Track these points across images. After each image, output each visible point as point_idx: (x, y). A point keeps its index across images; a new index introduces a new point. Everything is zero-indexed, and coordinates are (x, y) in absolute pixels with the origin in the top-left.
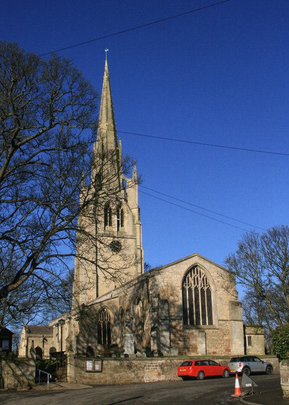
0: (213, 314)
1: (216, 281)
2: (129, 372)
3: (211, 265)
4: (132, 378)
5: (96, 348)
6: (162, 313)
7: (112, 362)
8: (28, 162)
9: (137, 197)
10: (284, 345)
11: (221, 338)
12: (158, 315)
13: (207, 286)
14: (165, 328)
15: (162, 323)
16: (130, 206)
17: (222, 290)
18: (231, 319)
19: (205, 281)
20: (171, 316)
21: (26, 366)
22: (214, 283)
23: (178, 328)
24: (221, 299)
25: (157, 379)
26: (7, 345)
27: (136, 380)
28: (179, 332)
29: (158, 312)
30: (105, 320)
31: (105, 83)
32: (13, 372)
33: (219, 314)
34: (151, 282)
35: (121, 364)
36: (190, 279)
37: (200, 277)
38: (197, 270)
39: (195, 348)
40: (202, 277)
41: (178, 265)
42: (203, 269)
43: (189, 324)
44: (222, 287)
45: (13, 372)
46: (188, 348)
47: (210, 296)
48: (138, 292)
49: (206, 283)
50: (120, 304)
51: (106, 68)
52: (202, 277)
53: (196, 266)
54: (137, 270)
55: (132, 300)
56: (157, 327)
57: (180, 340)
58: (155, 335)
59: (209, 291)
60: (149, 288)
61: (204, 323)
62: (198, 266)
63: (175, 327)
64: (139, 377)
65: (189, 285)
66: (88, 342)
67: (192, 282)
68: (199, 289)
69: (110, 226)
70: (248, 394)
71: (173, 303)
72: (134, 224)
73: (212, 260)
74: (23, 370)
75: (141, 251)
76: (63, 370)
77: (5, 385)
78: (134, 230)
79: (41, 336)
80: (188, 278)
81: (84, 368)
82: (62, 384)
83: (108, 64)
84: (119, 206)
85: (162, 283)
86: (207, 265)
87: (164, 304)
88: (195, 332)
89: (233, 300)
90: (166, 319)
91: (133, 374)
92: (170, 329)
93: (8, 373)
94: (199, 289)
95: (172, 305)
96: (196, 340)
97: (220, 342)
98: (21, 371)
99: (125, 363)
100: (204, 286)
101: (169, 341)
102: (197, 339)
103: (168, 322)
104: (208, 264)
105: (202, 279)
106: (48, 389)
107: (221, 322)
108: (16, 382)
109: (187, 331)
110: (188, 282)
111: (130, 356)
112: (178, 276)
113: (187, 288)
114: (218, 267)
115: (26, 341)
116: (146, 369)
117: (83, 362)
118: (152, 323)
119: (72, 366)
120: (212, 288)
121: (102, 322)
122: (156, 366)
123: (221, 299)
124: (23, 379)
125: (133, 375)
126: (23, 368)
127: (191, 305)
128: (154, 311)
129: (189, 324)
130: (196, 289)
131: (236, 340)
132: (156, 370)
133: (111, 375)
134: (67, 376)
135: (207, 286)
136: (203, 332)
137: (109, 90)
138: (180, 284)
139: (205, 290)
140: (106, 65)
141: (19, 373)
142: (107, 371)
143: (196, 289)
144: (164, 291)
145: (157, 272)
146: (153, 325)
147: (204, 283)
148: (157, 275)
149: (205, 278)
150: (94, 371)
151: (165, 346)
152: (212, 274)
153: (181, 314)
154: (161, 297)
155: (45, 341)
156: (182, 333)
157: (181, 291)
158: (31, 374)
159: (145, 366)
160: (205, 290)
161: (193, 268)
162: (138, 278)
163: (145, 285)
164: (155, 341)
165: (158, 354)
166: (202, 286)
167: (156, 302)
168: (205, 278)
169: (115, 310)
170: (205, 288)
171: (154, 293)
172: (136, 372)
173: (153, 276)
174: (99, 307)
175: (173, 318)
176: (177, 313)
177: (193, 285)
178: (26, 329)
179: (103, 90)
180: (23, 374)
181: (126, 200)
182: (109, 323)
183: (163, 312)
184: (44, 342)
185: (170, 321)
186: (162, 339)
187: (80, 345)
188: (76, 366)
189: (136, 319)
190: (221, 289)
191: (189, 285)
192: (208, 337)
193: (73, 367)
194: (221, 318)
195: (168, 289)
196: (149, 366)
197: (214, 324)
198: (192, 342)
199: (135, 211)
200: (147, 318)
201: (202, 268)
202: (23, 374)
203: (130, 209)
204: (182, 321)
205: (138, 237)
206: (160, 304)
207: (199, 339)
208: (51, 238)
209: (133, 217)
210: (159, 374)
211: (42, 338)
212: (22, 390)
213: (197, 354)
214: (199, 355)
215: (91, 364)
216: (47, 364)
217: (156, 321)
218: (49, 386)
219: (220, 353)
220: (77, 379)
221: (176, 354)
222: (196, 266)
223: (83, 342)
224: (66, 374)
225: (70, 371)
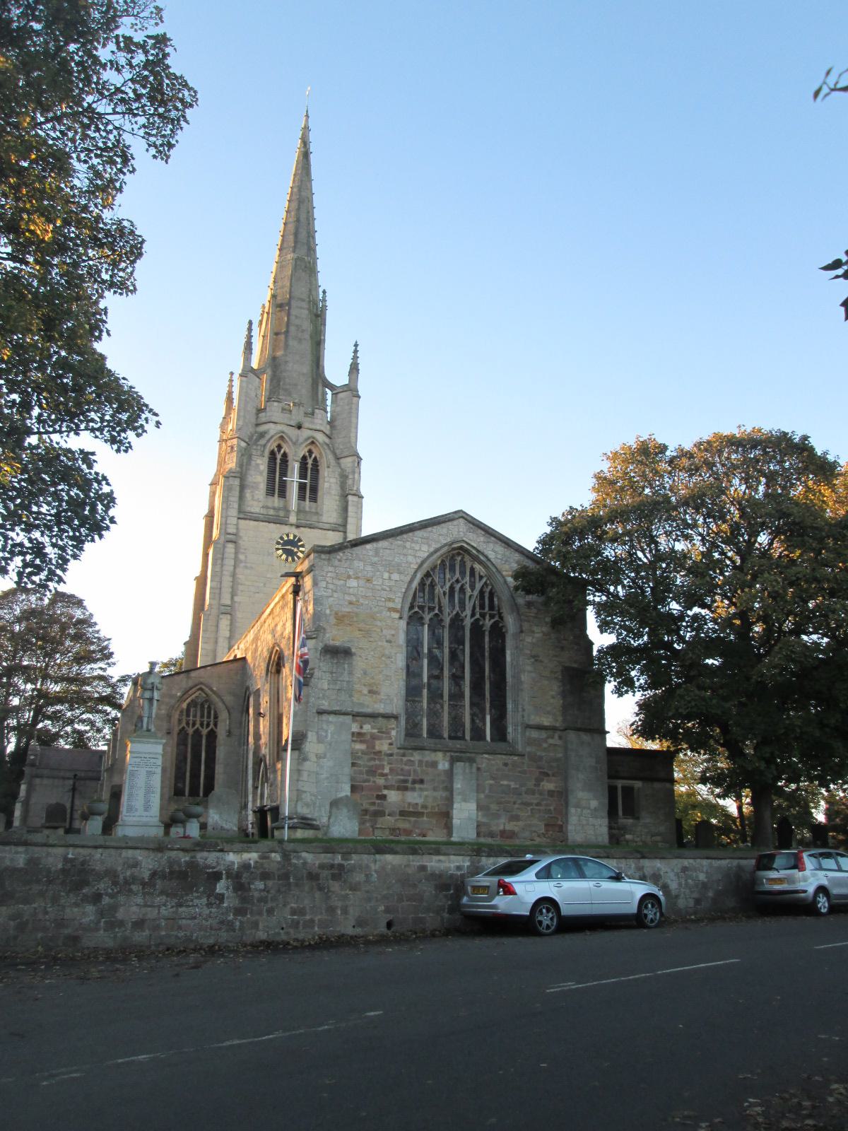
0: (510, 706)
11: (531, 784)
13: (492, 617)
40: (478, 586)
41: (398, 542)
42: (481, 563)
49: (492, 607)
59: (498, 632)
64: (121, 923)
67: (445, 601)
68: (468, 622)
91: (90, 908)
94: (468, 622)
97: (528, 798)
100: (483, 616)
105: (476, 593)
112: (396, 576)
131: (581, 794)
143: (457, 621)
147: (482, 607)
166: (478, 616)
170: (488, 623)
172: (106, 900)
177: (447, 610)
197: (510, 737)
201: (475, 559)
219: (527, 834)
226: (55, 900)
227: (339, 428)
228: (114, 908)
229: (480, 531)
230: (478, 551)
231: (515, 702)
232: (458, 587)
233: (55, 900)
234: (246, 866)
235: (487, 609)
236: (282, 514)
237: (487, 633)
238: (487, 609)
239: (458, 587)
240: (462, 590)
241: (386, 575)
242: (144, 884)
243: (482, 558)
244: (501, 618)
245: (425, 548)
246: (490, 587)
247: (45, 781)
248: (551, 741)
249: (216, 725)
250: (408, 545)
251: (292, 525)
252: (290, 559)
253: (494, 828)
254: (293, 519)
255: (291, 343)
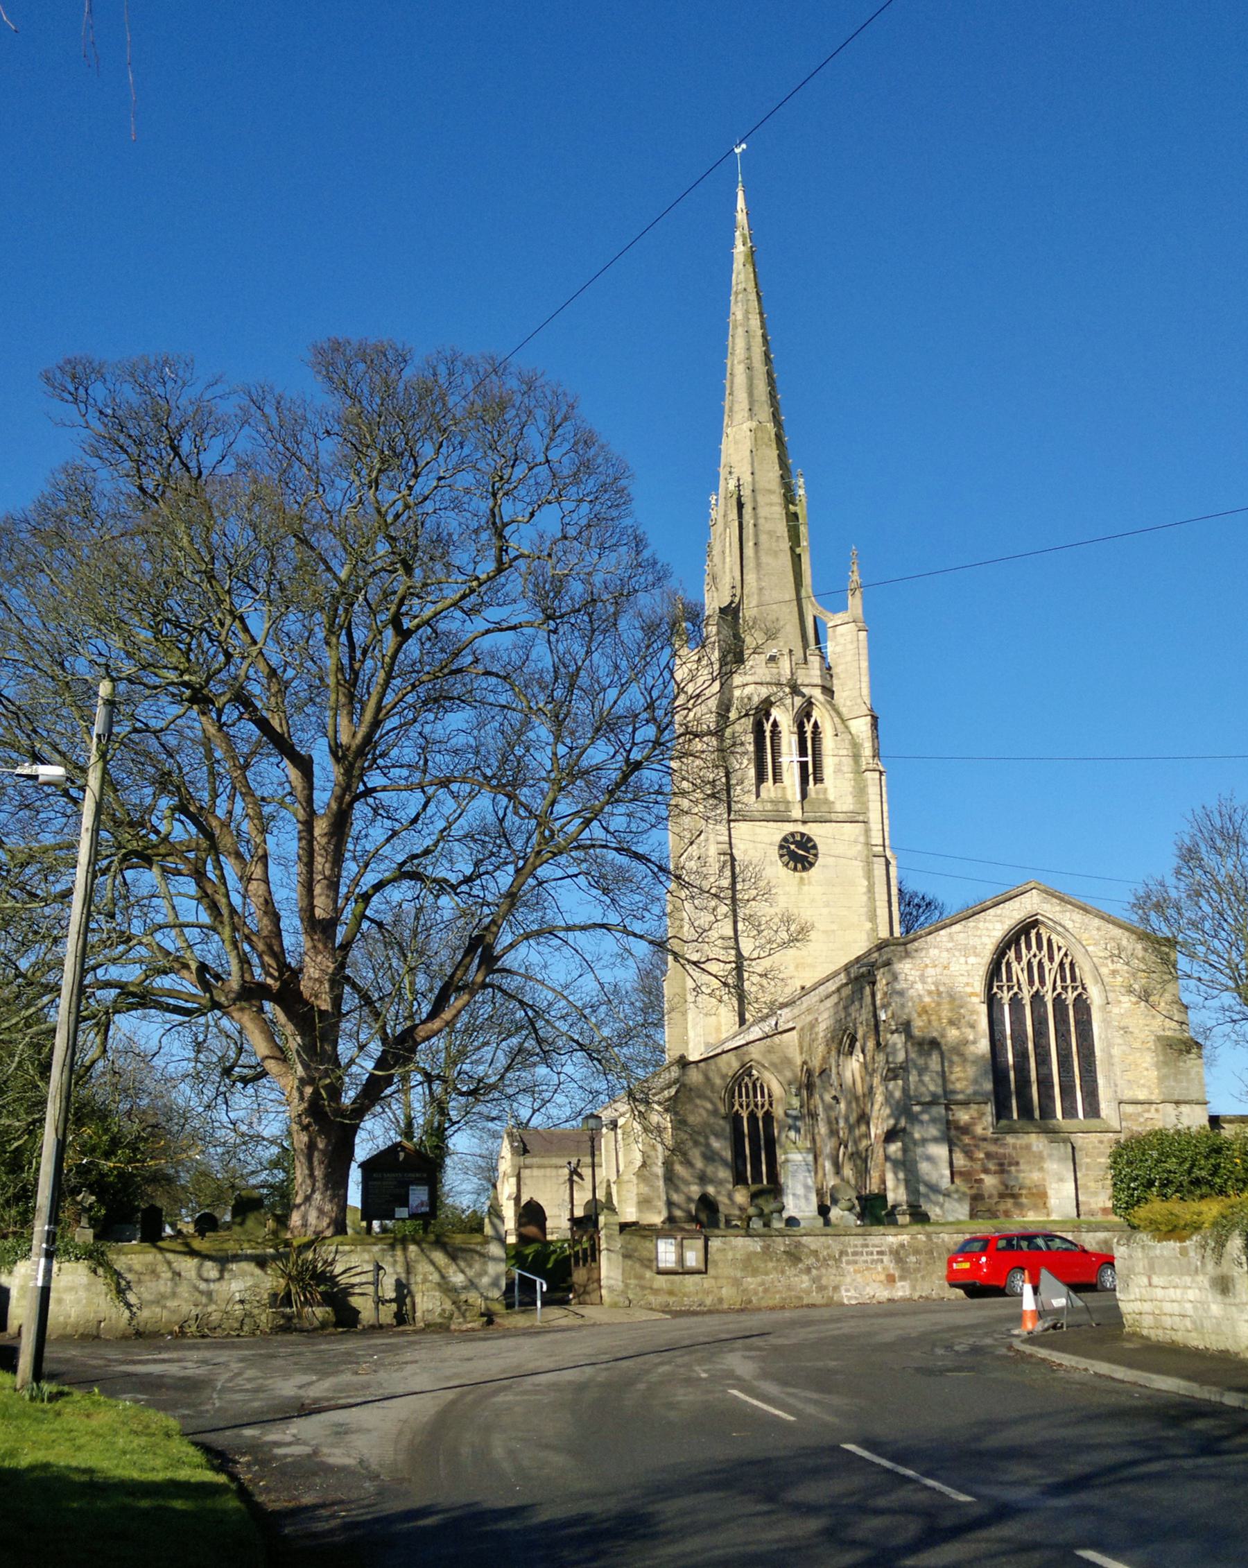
1: (1104, 971)
2: (790, 1272)
3: (1088, 919)
4: (802, 1290)
5: (730, 1197)
6: (921, 1081)
7: (740, 1242)
8: (446, 671)
9: (865, 679)
10: (1134, 1189)
12: (905, 1090)
13: (1074, 988)
14: (933, 1131)
15: (925, 1117)
16: (844, 711)
17: (1127, 1001)
18: (1161, 1098)
19: (1068, 970)
20: (954, 1092)
21: (477, 1257)
22: (1099, 979)
23: (979, 1130)
24: (1125, 1030)
25: (883, 1294)
26: (425, 1198)
27: (816, 1298)
28: (984, 1145)
29: (906, 1081)
30: (756, 1105)
31: (741, 275)
32: (443, 1277)
33: (1119, 1082)
34: (884, 982)
35: (766, 1249)
36: (1015, 966)
37: (1051, 959)
38: (1039, 936)
39: (1040, 1196)
40: (1057, 959)
41: (971, 923)
42: (1059, 934)
43: (1015, 1116)
44: (1130, 991)
45: (443, 1277)
46: (1014, 1196)
47: (1089, 1022)
48: (850, 1015)
49: (1073, 979)
50: (801, 1053)
51: (741, 217)
52: (1057, 959)
53: (1035, 924)
54: (875, 929)
55: (833, 1038)
56: (904, 1130)
57: (986, 1171)
58: (899, 1155)
59: (1082, 1006)
60: (878, 1002)
61: (1069, 1112)
62: (1043, 923)
63: (965, 1130)
65: (1010, 988)
66: (703, 1179)
67: (1024, 978)
68: (1049, 999)
69: (775, 782)
70: (1054, 1327)
71: (959, 1050)
72: (859, 772)
73: (1091, 903)
74: (470, 1273)
75: (888, 863)
76: (590, 1270)
77: (418, 1314)
78: (860, 791)
79: (564, 1162)
80: (1008, 964)
81: (650, 1261)
82: (587, 1311)
83: (746, 200)
84: (804, 714)
85: (919, 986)
86: (1071, 919)
87: (929, 1054)
88: (1037, 1142)
89: (1169, 1033)
90: (934, 1102)
91: (805, 1278)
92: (953, 1134)
93: (425, 1281)
94: (1049, 999)
95: (955, 1058)
96: (1041, 1169)
98: (463, 1272)
99: (780, 1245)
100: (1065, 988)
101: (947, 1172)
102: (1045, 1166)
103: (943, 1111)
104: (1078, 916)
106: (538, 1324)
107: (1129, 1109)
108: (448, 1306)
109: (1010, 1139)
110: (1009, 979)
111: (803, 1224)
112: (972, 960)
113: (1006, 996)
114: (1114, 923)
115: (513, 1180)
116: (848, 1263)
117: (648, 1244)
118: (889, 1117)
119: (613, 1255)
120: (1095, 995)
121: (745, 1115)
122: (881, 1253)
123: (1125, 1030)
124: (473, 1297)
125: (804, 1282)
126: (470, 1266)
127: (1022, 1055)
128: (895, 1078)
129: (1015, 1116)
130: (1037, 998)
132: (879, 1267)
133: (737, 1282)
134: (600, 1287)
135: (1074, 988)
136: (1066, 1141)
137: (753, 297)
138: (979, 986)
139: (1070, 1002)
140: (741, 203)
141: (458, 1279)
142: (723, 1268)
143: (1037, 998)
144: (925, 1011)
145: (901, 948)
146: (892, 1122)
147: (1063, 979)
148: (901, 959)
149: (1067, 961)
150: (682, 1271)
151: (934, 1189)
152: (1090, 949)
153: (988, 1086)
154: (916, 1033)
155: (575, 1178)
156: (992, 1148)
157: (983, 1009)
158: (495, 1284)
159: (842, 1253)
160: (1070, 1002)
161: (1026, 929)
162: (847, 968)
163: (867, 990)
164: (901, 1175)
165: (911, 1215)
166: (1059, 990)
167: (899, 1046)
168: (1067, 961)
169: (789, 1074)
170: (1070, 997)
171: (893, 1017)
172: (814, 1272)
173: (888, 963)
174: (736, 1065)
175: (960, 1097)
176: (975, 1082)
177: (1025, 987)
178: (511, 1143)
179: (732, 298)
180: (472, 1285)
181: (828, 691)
182: (768, 1117)
183: (926, 1079)
184: (571, 1181)
185: (947, 1108)
186: (924, 1167)
187: (677, 1190)
188: (627, 1256)
189: (849, 1104)
190: (1125, 999)
191: (1010, 988)
192: (1083, 1159)
193: (617, 1258)
194: (1128, 1095)
195: (939, 1004)
196: (855, 1254)
197: (1103, 1113)
198: (1029, 1176)
199: (862, 727)
200: (879, 1098)
201: (1053, 930)
202: (470, 1281)
203: (843, 721)
204: (989, 1109)
205: (874, 816)
206: (913, 1055)
207: (1052, 1166)
208: (540, 872)
209: (855, 746)
210: (891, 1279)
211: (566, 1171)
212: (464, 1327)
213: (1048, 1215)
214: (1054, 1217)
215: (673, 1249)
216: (555, 1251)
217: (903, 1108)
218: (542, 1314)
220: (631, 1297)
221: (962, 1218)
222: (1035, 924)
223: (688, 1184)
224: (599, 1280)
225: (610, 1269)
226: (783, 1272)
227: (842, 676)
228: (819, 1278)
229: (1054, 900)
230: (1055, 922)
231: (1107, 1078)
232: (1035, 962)
233: (783, 1272)
234: (902, 1246)
235: (1069, 981)
236: (782, 807)
237: (1071, 1007)
238: (1069, 981)
239: (1035, 962)
240: (1040, 964)
241: (962, 960)
242: (836, 1260)
243: (1059, 928)
244: (1084, 989)
245: (998, 926)
246: (1070, 958)
247: (536, 1172)
248: (1147, 1115)
249: (771, 1105)
250: (981, 925)
251: (796, 821)
252: (799, 866)
253: (1093, 1206)
254: (796, 813)
255: (764, 559)
